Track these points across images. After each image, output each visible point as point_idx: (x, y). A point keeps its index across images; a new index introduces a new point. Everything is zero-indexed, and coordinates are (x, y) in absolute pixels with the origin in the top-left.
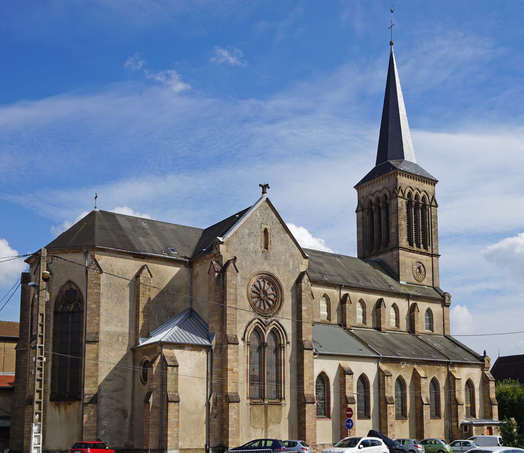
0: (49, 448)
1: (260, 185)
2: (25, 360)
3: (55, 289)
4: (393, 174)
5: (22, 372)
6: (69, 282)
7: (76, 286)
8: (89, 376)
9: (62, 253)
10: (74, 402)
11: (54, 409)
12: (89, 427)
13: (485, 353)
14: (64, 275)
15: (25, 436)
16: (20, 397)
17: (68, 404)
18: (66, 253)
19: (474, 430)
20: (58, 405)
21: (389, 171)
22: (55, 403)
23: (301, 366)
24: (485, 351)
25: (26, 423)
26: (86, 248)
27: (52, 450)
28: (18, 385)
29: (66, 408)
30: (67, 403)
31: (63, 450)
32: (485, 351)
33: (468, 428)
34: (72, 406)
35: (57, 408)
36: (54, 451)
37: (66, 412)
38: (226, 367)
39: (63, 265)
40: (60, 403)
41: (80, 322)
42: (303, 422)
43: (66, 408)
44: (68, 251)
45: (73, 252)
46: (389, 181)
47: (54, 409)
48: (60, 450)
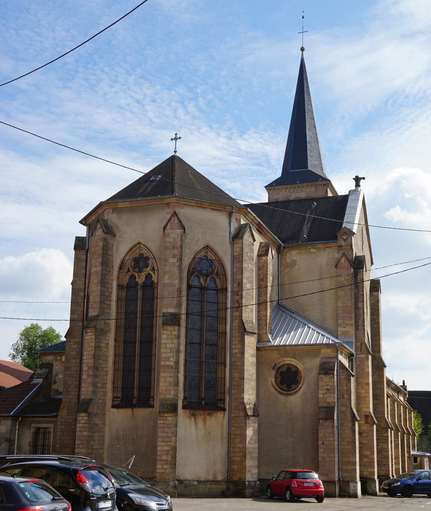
0: (182, 477)
1: (364, 178)
2: (106, 344)
3: (189, 253)
4: (323, 186)
5: (102, 362)
6: (207, 247)
7: (216, 254)
8: (248, 379)
9: (198, 207)
10: (217, 412)
11: (189, 420)
12: (252, 448)
13: (404, 383)
14: (200, 237)
15: (158, 458)
16: (100, 399)
17: (209, 415)
18: (204, 208)
19: (170, 458)
20: (194, 415)
21: (318, 181)
22: (190, 412)
23: (379, 386)
24: (404, 381)
25: (159, 439)
26: (236, 207)
27: (186, 480)
28: (98, 380)
29: (204, 420)
30: (206, 412)
31: (202, 479)
32: (404, 381)
33: (419, 459)
34: (213, 418)
35: (193, 419)
36: (189, 480)
37: (205, 425)
38: (366, 382)
39: (199, 223)
40: (196, 413)
41: (154, 299)
42: (384, 449)
43: (204, 420)
44: (223, 208)
45: (213, 209)
46: (316, 191)
47: (188, 420)
48: (198, 479)
